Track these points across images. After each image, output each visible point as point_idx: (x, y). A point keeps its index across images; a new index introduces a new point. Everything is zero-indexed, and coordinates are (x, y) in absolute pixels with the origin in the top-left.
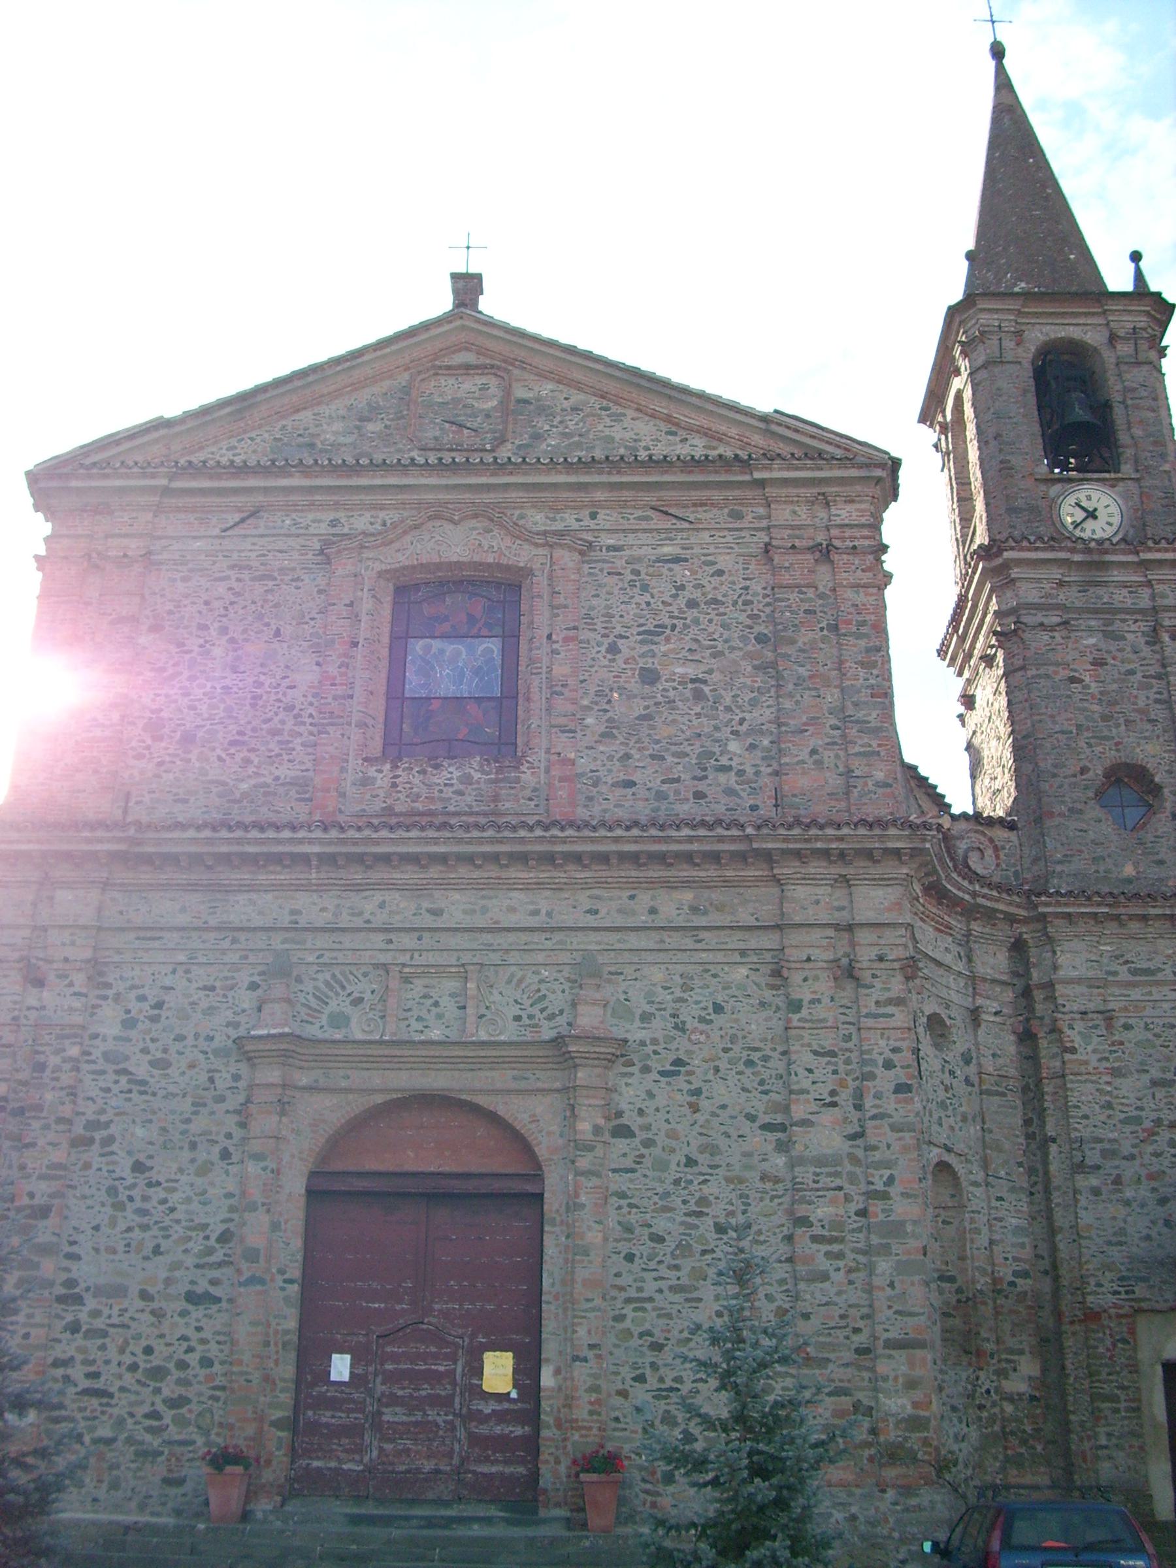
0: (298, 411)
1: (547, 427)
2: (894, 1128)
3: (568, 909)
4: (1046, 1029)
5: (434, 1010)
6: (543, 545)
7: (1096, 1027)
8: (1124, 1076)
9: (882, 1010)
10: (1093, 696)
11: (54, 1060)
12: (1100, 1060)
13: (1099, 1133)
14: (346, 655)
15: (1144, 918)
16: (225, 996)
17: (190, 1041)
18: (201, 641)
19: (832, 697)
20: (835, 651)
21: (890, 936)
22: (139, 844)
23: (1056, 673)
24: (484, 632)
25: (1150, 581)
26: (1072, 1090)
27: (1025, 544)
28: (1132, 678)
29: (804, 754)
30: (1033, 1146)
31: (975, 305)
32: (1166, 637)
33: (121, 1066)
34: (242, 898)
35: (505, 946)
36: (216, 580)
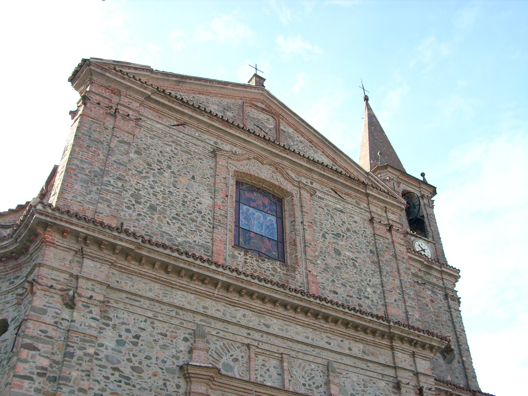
0: (200, 94)
1: (292, 144)
3: (319, 339)
5: (268, 373)
6: (296, 186)
11: (79, 353)
14: (224, 198)
16: (172, 341)
17: (154, 360)
18: (159, 167)
22: (139, 248)
24: (269, 212)
25: (443, 278)
27: (413, 252)
31: (387, 168)
33: (115, 366)
34: (180, 293)
35: (297, 350)
36: (166, 144)
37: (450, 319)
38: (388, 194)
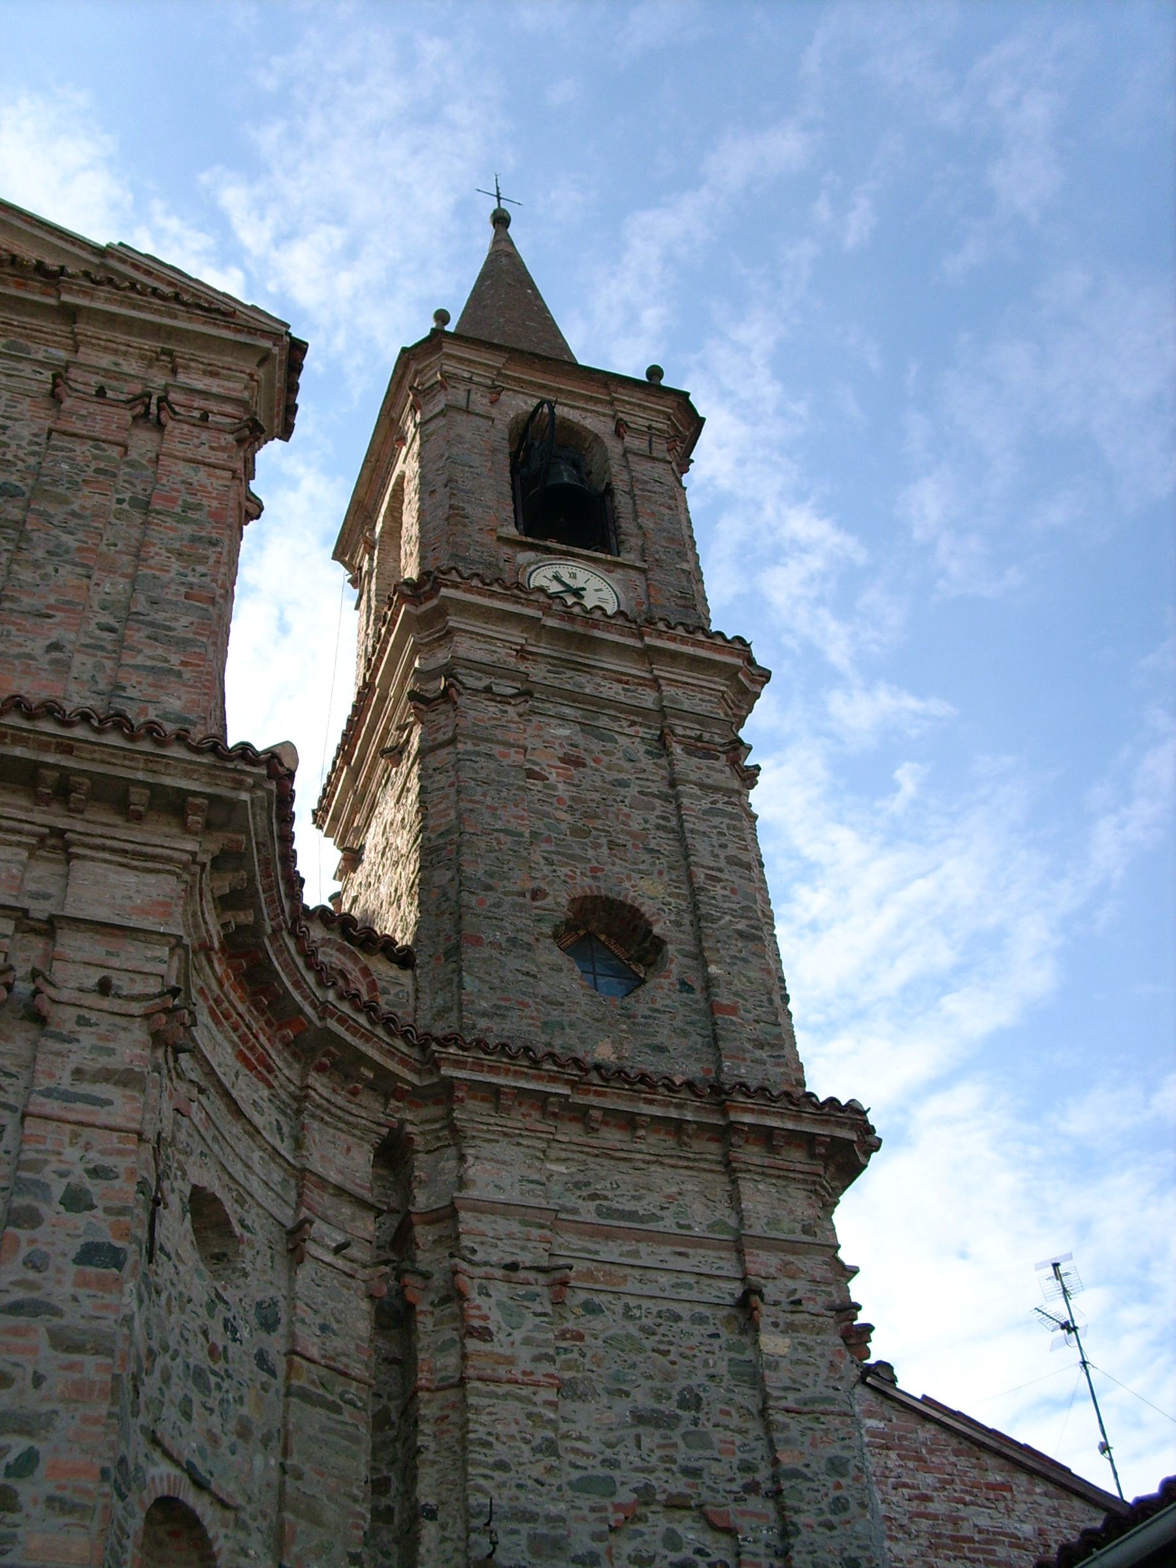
2: (63, 1342)
4: (433, 1297)
7: (533, 1297)
8: (583, 1397)
9: (85, 1088)
10: (560, 800)
12: (537, 1359)
13: (526, 1500)
15: (630, 1122)
19: (113, 587)
20: (136, 533)
21: (132, 955)
23: (505, 755)
25: (656, 679)
26: (478, 1410)
28: (622, 791)
29: (37, 646)
30: (386, 1536)
31: (439, 348)
32: (677, 749)
37: (674, 823)
38: (176, 298)
